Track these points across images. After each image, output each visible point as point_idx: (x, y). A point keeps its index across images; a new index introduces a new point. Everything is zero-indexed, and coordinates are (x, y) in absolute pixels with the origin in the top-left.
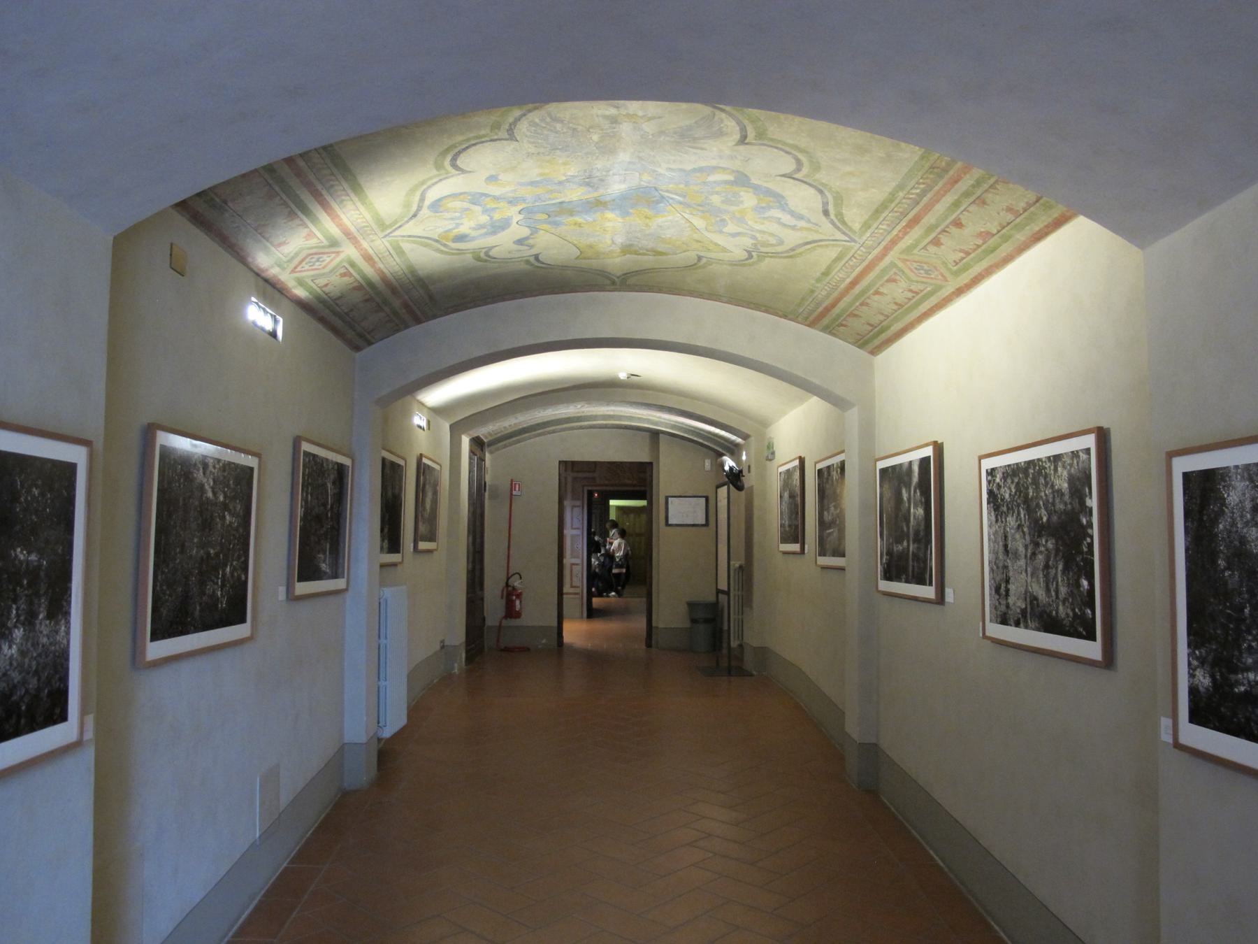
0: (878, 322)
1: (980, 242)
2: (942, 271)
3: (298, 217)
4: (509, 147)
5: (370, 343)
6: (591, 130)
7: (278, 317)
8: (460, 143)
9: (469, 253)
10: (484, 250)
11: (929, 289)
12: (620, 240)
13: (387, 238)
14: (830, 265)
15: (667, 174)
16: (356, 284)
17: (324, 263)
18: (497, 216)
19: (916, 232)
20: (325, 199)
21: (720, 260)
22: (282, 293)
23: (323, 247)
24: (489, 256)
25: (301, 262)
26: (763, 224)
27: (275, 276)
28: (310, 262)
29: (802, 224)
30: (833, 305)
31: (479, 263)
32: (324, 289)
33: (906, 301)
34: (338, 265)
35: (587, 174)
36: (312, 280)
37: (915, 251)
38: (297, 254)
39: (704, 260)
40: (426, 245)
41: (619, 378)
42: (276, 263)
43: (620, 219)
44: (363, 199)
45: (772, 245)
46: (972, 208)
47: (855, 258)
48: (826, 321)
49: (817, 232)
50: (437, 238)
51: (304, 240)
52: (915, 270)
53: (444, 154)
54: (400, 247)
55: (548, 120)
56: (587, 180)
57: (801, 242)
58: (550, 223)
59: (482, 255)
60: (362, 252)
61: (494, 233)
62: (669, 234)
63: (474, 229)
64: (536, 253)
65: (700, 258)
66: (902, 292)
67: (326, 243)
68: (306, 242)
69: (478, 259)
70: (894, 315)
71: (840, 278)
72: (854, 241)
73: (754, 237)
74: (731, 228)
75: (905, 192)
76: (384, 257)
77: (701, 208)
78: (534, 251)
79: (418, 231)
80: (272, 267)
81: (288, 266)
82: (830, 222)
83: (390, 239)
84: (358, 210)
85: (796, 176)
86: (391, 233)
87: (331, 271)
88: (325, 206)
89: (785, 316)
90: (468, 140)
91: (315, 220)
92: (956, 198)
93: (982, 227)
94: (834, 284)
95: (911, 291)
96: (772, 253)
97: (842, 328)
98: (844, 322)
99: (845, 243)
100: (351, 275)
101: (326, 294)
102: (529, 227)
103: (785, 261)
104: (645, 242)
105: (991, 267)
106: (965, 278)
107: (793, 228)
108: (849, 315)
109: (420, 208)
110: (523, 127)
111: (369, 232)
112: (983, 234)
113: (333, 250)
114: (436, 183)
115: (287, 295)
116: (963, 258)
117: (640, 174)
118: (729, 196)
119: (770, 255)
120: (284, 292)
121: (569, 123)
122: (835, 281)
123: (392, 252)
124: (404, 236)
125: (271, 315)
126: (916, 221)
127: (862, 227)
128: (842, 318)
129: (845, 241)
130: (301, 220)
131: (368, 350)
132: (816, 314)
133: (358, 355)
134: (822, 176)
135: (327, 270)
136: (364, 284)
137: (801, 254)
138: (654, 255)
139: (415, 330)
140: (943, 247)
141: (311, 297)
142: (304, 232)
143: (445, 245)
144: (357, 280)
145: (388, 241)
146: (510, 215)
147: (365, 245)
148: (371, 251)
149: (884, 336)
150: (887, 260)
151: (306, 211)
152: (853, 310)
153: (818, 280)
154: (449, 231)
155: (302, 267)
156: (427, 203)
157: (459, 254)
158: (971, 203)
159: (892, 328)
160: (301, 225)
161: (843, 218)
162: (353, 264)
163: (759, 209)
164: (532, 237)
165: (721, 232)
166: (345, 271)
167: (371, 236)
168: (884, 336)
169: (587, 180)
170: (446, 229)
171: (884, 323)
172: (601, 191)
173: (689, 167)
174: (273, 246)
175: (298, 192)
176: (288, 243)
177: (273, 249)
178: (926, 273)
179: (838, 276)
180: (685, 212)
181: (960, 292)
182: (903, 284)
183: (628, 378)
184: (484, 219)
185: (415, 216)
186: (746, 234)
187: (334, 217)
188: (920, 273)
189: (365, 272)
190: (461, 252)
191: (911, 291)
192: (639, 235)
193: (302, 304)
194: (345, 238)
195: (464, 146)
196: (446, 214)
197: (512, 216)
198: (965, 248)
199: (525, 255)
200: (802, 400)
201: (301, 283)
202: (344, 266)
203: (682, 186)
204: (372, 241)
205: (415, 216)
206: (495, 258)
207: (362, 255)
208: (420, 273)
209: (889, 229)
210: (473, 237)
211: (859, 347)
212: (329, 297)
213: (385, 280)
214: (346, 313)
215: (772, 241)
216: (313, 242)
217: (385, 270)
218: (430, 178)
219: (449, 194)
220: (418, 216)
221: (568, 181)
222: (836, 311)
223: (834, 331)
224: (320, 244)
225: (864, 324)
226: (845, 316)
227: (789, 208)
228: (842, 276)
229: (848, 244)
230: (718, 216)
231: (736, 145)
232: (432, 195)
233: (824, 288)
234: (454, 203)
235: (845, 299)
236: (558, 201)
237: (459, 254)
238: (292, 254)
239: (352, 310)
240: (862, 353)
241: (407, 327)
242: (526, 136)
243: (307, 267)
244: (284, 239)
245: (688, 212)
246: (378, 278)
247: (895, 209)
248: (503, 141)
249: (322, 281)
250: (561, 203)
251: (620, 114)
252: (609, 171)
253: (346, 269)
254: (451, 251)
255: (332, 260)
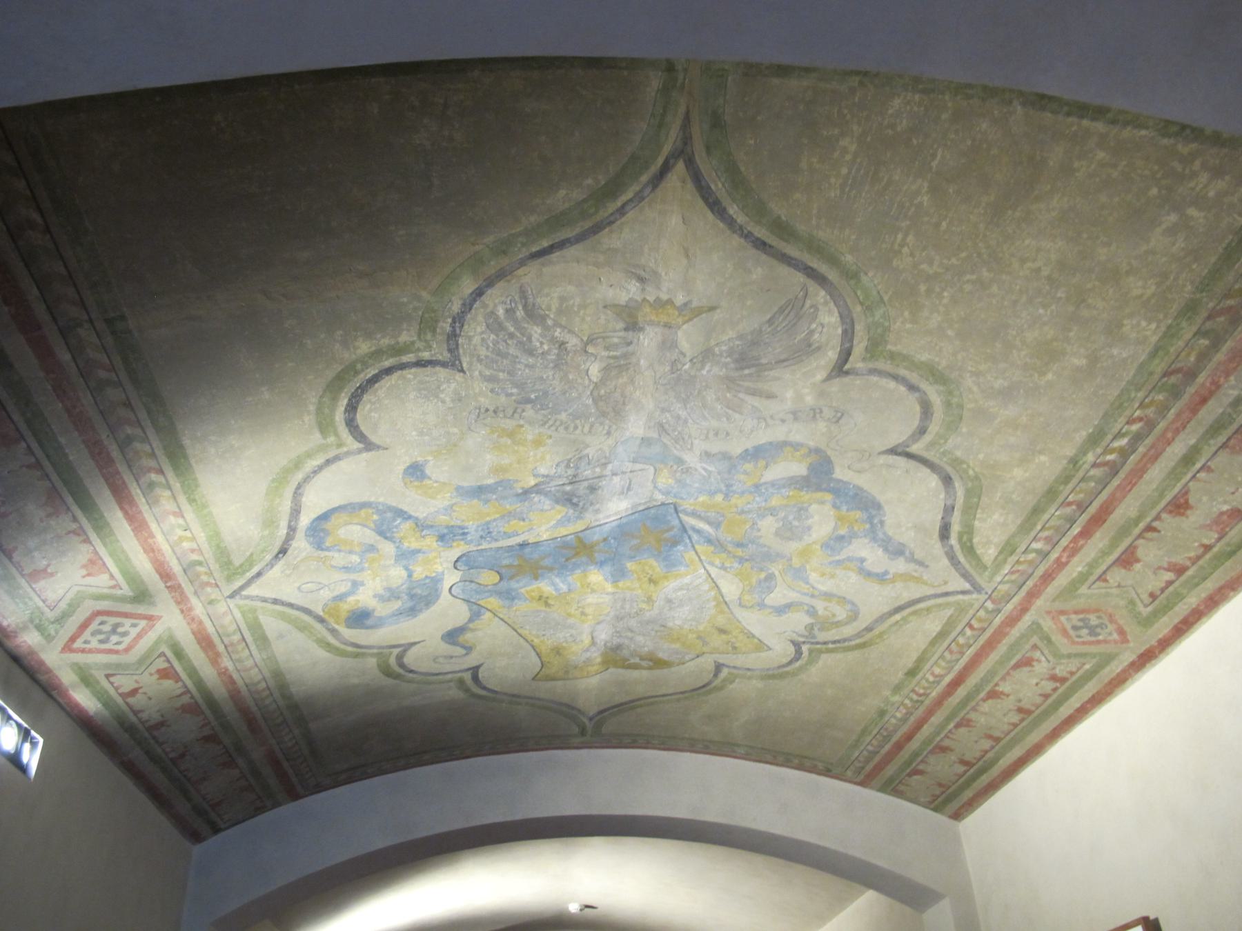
0: (978, 755)
1: (1210, 537)
2: (1121, 622)
3: (68, 509)
4: (448, 383)
5: (216, 830)
6: (591, 349)
7: (33, 733)
8: (365, 361)
9: (372, 655)
10: (396, 651)
11: (1087, 667)
12: (604, 635)
13: (237, 600)
14: (925, 651)
15: (699, 466)
16: (186, 699)
17: (127, 640)
18: (419, 572)
19: (1099, 540)
20: (118, 473)
21: (749, 669)
22: (51, 696)
23: (123, 599)
24: (402, 665)
25: (84, 626)
26: (832, 576)
27: (32, 653)
28: (100, 632)
29: (900, 566)
30: (909, 737)
31: (389, 681)
32: (131, 700)
33: (1041, 699)
34: (151, 650)
35: (570, 472)
36: (107, 676)
37: (1083, 590)
38: (73, 607)
39: (725, 672)
40: (302, 628)
41: (570, 912)
42: (31, 621)
43: (609, 588)
44: (190, 489)
45: (838, 624)
46: (1223, 457)
47: (971, 627)
48: (890, 770)
49: (918, 580)
50: (321, 614)
51: (84, 572)
52: (1072, 632)
53: (334, 387)
54: (260, 626)
55: (520, 313)
56: (568, 488)
57: (886, 609)
58: (499, 594)
59: (392, 661)
60: (194, 626)
61: (412, 611)
62: (680, 618)
63: (381, 598)
64: (475, 664)
65: (719, 667)
66: (1037, 684)
67: (126, 590)
68: (89, 580)
69: (387, 672)
70: (1012, 734)
71: (936, 676)
72: (977, 588)
73: (812, 612)
74: (779, 596)
75: (1099, 450)
76: (232, 644)
77: (739, 552)
78: (472, 661)
79: (288, 592)
80: (25, 628)
81: (57, 632)
82: (947, 553)
83: (242, 602)
84: (183, 517)
85: (915, 448)
86: (242, 588)
87: (141, 661)
88: (121, 495)
89: (827, 772)
90: (378, 354)
91: (101, 527)
92: (1192, 442)
93: (1225, 502)
94: (922, 691)
95: (1053, 678)
96: (834, 642)
97: (916, 777)
98: (921, 767)
99: (960, 597)
100: (177, 678)
101: (135, 713)
102: (467, 601)
103: (851, 656)
104: (640, 639)
105: (1221, 589)
106: (1164, 626)
107: (881, 578)
108: (931, 752)
109: (289, 538)
110: (476, 332)
111: (205, 578)
112: (1225, 517)
113: (141, 609)
114: (320, 468)
115: (60, 700)
116: (1169, 583)
117: (656, 470)
118: (791, 518)
119: (831, 646)
120: (54, 693)
121: (557, 324)
122: (926, 685)
123: (249, 639)
124: (264, 600)
125: (19, 725)
126: (1098, 520)
127: (1001, 552)
128: (920, 759)
129: (963, 592)
130: (75, 519)
131: (213, 842)
132: (877, 759)
133: (197, 850)
134: (957, 444)
135: (133, 657)
136: (200, 701)
137: (881, 635)
138: (650, 668)
139: (289, 809)
140: (1138, 566)
141: (106, 713)
142: (83, 553)
143: (333, 632)
144: (188, 691)
145: (239, 607)
146: (440, 569)
147: (199, 609)
148: (210, 629)
149: (985, 779)
150: (1027, 619)
151: (87, 504)
152: (942, 740)
153: (897, 689)
154: (341, 598)
155: (86, 642)
156: (305, 521)
157: (356, 655)
158: (1221, 447)
159: (1001, 762)
160: (74, 532)
161: (971, 540)
162: (179, 653)
163: (837, 541)
164: (471, 625)
165: (761, 605)
166: (166, 665)
167: (209, 589)
168: (985, 779)
169: (568, 488)
170: (336, 593)
171: (990, 755)
172: (589, 518)
173: (736, 448)
174: (23, 576)
175: (62, 440)
176: (52, 575)
177: (23, 582)
178: (1090, 634)
179: (933, 674)
180: (712, 564)
181: (1146, 658)
182: (1042, 667)
183: (581, 910)
184: (397, 575)
185: (283, 551)
186: (801, 604)
187: (139, 525)
188: (1079, 637)
189: (202, 674)
190: (359, 651)
191: (1053, 678)
192: (633, 623)
193: (84, 722)
194: (161, 585)
195: (371, 372)
196: (336, 555)
197: (443, 573)
198: (1179, 559)
199: (457, 668)
200: (839, 903)
201: (86, 679)
202: (163, 654)
203: (719, 498)
204: (211, 602)
205: (283, 551)
206: (411, 671)
207: (194, 633)
208: (293, 689)
209: (1048, 548)
210: (380, 618)
211: (936, 810)
212: (140, 720)
213: (235, 695)
214: (171, 760)
215: (841, 613)
216: (101, 582)
217: (235, 676)
218: (309, 455)
219: (343, 502)
220: (289, 552)
221: (537, 489)
222: (914, 745)
223: (902, 788)
224: (114, 591)
225: (955, 762)
226: (925, 753)
227: (885, 533)
228: (939, 671)
229: (966, 597)
230: (762, 570)
231: (829, 378)
232: (316, 501)
233: (902, 703)
234: (349, 527)
235: (933, 719)
236: (519, 540)
237: (356, 655)
238: (63, 605)
239: (183, 756)
240: (940, 819)
241: (277, 804)
242: (480, 360)
243: (94, 644)
244: (45, 562)
245: (717, 562)
246: (226, 695)
247: (1071, 498)
248: (438, 369)
249: (126, 682)
250: (523, 545)
251: (644, 300)
252: (605, 465)
253: (168, 661)
254: (343, 647)
255: (139, 636)
